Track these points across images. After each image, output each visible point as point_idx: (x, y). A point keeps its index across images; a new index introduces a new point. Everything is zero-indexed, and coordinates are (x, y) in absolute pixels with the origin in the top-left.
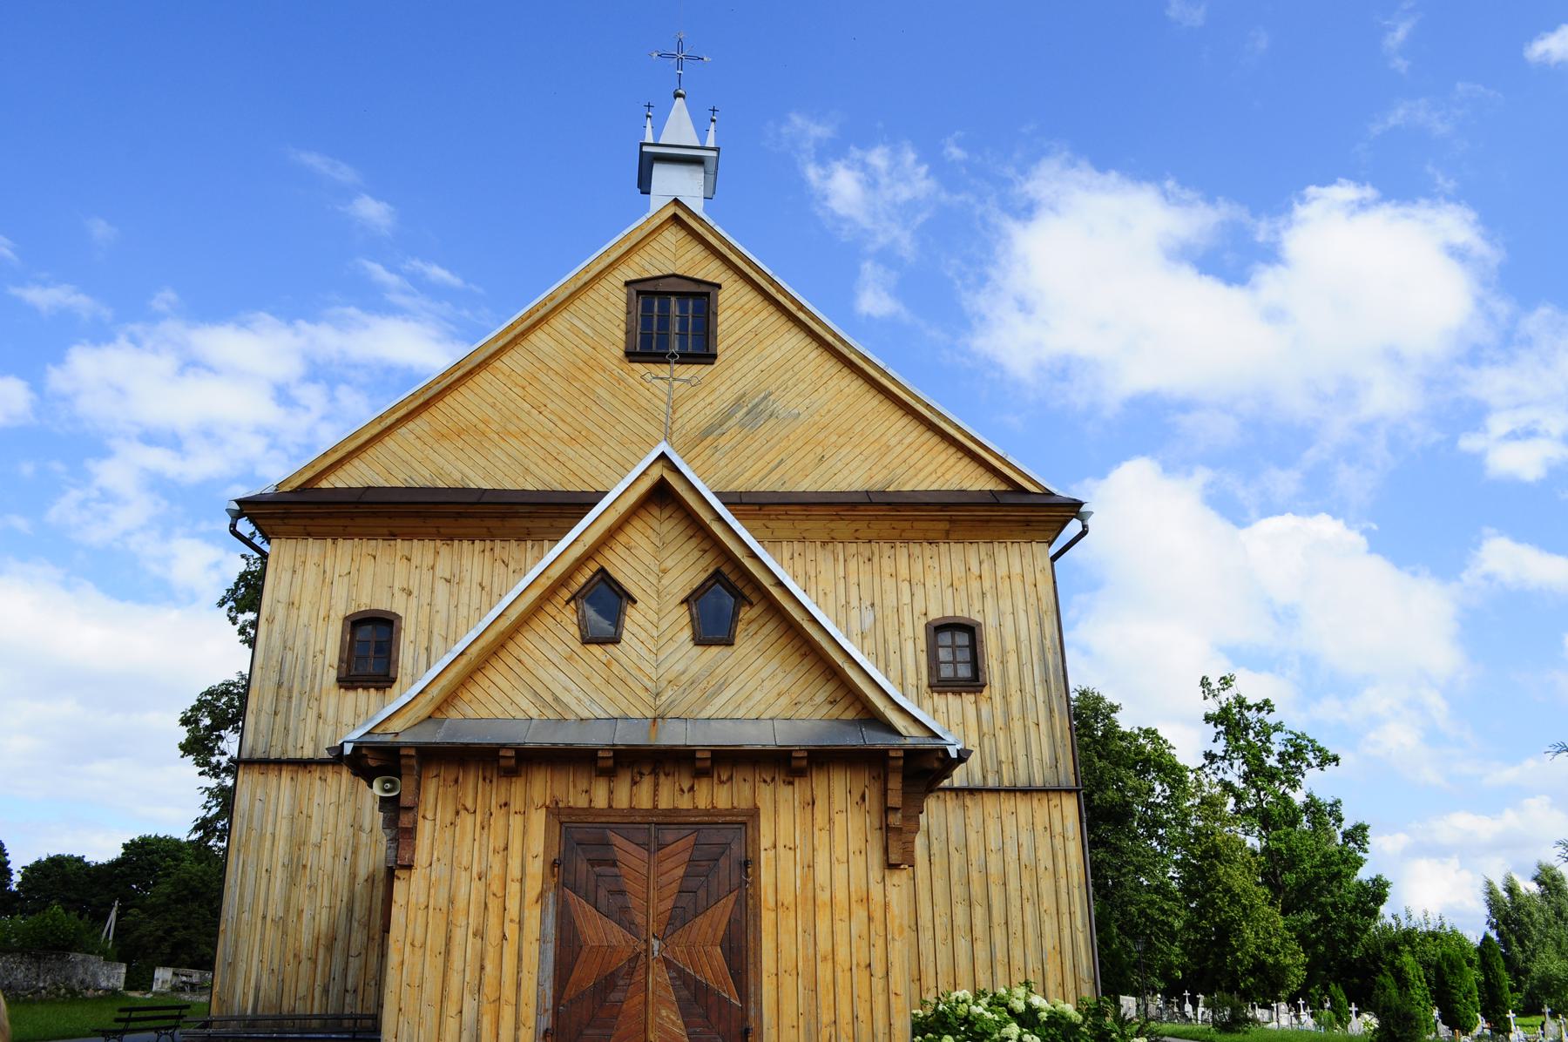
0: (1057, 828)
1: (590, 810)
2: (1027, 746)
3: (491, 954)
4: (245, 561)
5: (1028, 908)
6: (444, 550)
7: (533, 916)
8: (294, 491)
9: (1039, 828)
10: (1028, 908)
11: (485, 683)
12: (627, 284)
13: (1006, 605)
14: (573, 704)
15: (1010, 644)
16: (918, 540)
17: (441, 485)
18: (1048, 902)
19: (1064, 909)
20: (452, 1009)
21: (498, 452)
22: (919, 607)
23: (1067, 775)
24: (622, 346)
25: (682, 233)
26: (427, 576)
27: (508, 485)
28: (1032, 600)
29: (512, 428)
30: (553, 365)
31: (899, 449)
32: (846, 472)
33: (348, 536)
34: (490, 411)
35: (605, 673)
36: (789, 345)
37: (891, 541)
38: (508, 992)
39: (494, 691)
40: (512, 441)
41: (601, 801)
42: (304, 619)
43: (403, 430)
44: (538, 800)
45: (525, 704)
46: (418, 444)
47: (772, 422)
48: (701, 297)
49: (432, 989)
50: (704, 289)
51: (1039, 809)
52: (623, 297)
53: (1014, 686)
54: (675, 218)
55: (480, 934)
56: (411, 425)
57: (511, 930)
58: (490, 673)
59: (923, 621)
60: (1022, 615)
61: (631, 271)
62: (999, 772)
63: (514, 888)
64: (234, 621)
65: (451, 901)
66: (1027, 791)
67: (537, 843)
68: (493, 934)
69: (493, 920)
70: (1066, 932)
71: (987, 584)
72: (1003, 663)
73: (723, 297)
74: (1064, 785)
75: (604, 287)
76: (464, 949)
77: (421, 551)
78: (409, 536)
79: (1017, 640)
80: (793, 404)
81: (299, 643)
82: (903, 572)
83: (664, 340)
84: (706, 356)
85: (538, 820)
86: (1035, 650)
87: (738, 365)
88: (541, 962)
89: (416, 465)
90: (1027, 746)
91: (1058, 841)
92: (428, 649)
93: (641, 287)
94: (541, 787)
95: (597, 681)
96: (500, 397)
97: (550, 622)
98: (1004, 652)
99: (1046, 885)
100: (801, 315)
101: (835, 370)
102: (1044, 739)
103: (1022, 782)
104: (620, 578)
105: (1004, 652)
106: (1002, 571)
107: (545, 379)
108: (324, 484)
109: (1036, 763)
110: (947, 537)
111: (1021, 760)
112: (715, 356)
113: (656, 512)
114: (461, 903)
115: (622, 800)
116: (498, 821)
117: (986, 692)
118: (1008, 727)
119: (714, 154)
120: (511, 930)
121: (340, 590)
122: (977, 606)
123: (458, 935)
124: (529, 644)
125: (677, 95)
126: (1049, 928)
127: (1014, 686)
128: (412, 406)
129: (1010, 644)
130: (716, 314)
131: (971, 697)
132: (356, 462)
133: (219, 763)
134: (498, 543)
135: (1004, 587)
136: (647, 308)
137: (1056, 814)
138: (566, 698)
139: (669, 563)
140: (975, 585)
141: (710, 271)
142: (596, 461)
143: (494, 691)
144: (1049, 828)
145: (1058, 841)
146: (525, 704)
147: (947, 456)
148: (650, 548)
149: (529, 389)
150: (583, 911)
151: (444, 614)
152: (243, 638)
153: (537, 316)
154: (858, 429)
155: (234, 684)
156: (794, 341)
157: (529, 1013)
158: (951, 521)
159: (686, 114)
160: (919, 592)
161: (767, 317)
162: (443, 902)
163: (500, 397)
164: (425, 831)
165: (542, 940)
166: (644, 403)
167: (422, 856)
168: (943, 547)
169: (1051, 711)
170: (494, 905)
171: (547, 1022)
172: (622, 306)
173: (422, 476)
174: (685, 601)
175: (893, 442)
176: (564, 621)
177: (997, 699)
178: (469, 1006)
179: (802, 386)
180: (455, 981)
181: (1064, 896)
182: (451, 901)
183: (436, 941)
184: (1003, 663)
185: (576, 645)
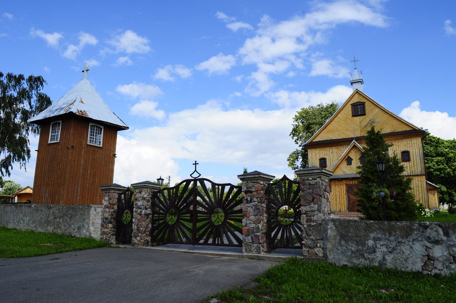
0: (422, 180)
1: (350, 184)
2: (417, 169)
3: (341, 200)
4: (293, 126)
5: (417, 192)
6: (330, 148)
7: (345, 196)
8: (310, 143)
9: (419, 181)
10: (417, 192)
11: (337, 171)
12: (351, 104)
13: (414, 148)
14: (347, 172)
15: (414, 154)
16: (399, 139)
17: (329, 139)
18: (420, 191)
19: (423, 192)
20: (337, 206)
21: (336, 133)
22: (400, 149)
23: (423, 172)
24: (351, 114)
25: (359, 94)
26: (329, 152)
27: (338, 138)
28: (418, 147)
29: (337, 130)
30: (342, 119)
31: (395, 125)
32: (387, 130)
33: (318, 148)
34: (334, 127)
35: (350, 168)
36: (377, 111)
37: (395, 140)
38: (343, 204)
39: (338, 171)
40: (338, 132)
41: (351, 183)
42: (314, 160)
43: (322, 132)
44: (344, 183)
45: (342, 173)
46: (325, 134)
47: (375, 123)
48: (363, 104)
49: (335, 204)
50: (363, 103)
51: (419, 178)
52: (351, 107)
53: (415, 160)
54: (357, 92)
55: (339, 198)
56: (323, 131)
57: (343, 197)
58: (337, 169)
59: (400, 152)
60: (416, 149)
61: (351, 102)
62: (413, 173)
63: (343, 193)
64: (293, 139)
65: (336, 195)
66: (417, 175)
67: (345, 188)
68: (341, 198)
69: (341, 196)
70: (423, 195)
71: (410, 145)
72: (413, 157)
73: (366, 104)
74: (423, 174)
75: (347, 105)
76: (338, 200)
77: (328, 149)
78: (326, 147)
79: (416, 153)
80: (378, 120)
81: (314, 163)
82: (397, 144)
83: (358, 112)
84: (364, 114)
85: (344, 186)
86: (418, 154)
87: (369, 115)
88: (346, 201)
89: (325, 137)
90: (417, 169)
91: (422, 182)
92: (330, 162)
93: (353, 105)
94: (344, 182)
95: (349, 170)
96: (335, 125)
97: (343, 163)
98: (413, 155)
99: (420, 189)
100: (378, 106)
101: (384, 114)
102: (420, 168)
103: (416, 174)
104: (351, 157)
105: (413, 155)
106: (413, 143)
107: (341, 122)
108: (313, 141)
109: (418, 171)
110: (404, 138)
111: (416, 171)
112: (366, 114)
113: (354, 148)
114: (337, 195)
115: (354, 183)
116: (340, 186)
117: (410, 161)
118: (414, 166)
119: (362, 80)
120: (343, 197)
121: (318, 156)
122: (409, 148)
123: (337, 198)
124: (341, 166)
125: (355, 69)
126: (421, 195)
127: (415, 160)
128: (323, 128)
129: (414, 154)
130: (365, 107)
131: (408, 162)
132: (317, 137)
133: (295, 167)
134: (338, 147)
135: (413, 145)
136: (355, 108)
137: (422, 179)
138: (346, 172)
139: (357, 155)
140: (409, 145)
141: (363, 100)
142: (349, 133)
143: (338, 171)
144: (421, 181)
145: (422, 182)
146: (342, 173)
147: (403, 125)
148: (354, 153)
149: (339, 123)
150: (350, 195)
151: (332, 157)
152: (295, 143)
153: (338, 112)
154: (389, 123)
155: (295, 152)
156: (378, 110)
157: (346, 206)
158: (404, 136)
159: (357, 72)
160: (400, 147)
161: (373, 106)
162: (335, 195)
163: (335, 125)
164: (332, 187)
165: (346, 198)
166: (355, 123)
167: (332, 190)
168: (403, 140)
169: (421, 163)
170: (341, 195)
171: (348, 207)
172: (351, 108)
173: (326, 138)
174: (359, 159)
175: (395, 124)
176: (345, 163)
177: (412, 162)
178: (339, 205)
179: (379, 117)
180: (337, 203)
181: (423, 190)
182: (336, 195)
183: (335, 199)
184: (413, 157)
185: (346, 165)
